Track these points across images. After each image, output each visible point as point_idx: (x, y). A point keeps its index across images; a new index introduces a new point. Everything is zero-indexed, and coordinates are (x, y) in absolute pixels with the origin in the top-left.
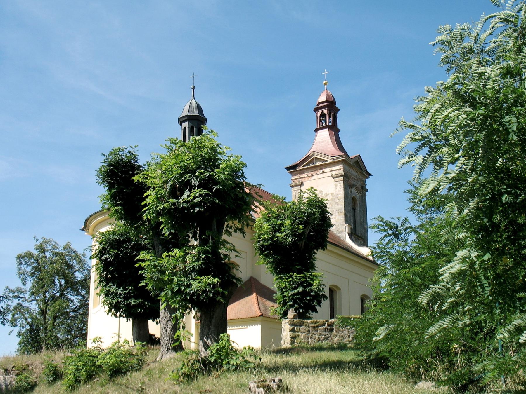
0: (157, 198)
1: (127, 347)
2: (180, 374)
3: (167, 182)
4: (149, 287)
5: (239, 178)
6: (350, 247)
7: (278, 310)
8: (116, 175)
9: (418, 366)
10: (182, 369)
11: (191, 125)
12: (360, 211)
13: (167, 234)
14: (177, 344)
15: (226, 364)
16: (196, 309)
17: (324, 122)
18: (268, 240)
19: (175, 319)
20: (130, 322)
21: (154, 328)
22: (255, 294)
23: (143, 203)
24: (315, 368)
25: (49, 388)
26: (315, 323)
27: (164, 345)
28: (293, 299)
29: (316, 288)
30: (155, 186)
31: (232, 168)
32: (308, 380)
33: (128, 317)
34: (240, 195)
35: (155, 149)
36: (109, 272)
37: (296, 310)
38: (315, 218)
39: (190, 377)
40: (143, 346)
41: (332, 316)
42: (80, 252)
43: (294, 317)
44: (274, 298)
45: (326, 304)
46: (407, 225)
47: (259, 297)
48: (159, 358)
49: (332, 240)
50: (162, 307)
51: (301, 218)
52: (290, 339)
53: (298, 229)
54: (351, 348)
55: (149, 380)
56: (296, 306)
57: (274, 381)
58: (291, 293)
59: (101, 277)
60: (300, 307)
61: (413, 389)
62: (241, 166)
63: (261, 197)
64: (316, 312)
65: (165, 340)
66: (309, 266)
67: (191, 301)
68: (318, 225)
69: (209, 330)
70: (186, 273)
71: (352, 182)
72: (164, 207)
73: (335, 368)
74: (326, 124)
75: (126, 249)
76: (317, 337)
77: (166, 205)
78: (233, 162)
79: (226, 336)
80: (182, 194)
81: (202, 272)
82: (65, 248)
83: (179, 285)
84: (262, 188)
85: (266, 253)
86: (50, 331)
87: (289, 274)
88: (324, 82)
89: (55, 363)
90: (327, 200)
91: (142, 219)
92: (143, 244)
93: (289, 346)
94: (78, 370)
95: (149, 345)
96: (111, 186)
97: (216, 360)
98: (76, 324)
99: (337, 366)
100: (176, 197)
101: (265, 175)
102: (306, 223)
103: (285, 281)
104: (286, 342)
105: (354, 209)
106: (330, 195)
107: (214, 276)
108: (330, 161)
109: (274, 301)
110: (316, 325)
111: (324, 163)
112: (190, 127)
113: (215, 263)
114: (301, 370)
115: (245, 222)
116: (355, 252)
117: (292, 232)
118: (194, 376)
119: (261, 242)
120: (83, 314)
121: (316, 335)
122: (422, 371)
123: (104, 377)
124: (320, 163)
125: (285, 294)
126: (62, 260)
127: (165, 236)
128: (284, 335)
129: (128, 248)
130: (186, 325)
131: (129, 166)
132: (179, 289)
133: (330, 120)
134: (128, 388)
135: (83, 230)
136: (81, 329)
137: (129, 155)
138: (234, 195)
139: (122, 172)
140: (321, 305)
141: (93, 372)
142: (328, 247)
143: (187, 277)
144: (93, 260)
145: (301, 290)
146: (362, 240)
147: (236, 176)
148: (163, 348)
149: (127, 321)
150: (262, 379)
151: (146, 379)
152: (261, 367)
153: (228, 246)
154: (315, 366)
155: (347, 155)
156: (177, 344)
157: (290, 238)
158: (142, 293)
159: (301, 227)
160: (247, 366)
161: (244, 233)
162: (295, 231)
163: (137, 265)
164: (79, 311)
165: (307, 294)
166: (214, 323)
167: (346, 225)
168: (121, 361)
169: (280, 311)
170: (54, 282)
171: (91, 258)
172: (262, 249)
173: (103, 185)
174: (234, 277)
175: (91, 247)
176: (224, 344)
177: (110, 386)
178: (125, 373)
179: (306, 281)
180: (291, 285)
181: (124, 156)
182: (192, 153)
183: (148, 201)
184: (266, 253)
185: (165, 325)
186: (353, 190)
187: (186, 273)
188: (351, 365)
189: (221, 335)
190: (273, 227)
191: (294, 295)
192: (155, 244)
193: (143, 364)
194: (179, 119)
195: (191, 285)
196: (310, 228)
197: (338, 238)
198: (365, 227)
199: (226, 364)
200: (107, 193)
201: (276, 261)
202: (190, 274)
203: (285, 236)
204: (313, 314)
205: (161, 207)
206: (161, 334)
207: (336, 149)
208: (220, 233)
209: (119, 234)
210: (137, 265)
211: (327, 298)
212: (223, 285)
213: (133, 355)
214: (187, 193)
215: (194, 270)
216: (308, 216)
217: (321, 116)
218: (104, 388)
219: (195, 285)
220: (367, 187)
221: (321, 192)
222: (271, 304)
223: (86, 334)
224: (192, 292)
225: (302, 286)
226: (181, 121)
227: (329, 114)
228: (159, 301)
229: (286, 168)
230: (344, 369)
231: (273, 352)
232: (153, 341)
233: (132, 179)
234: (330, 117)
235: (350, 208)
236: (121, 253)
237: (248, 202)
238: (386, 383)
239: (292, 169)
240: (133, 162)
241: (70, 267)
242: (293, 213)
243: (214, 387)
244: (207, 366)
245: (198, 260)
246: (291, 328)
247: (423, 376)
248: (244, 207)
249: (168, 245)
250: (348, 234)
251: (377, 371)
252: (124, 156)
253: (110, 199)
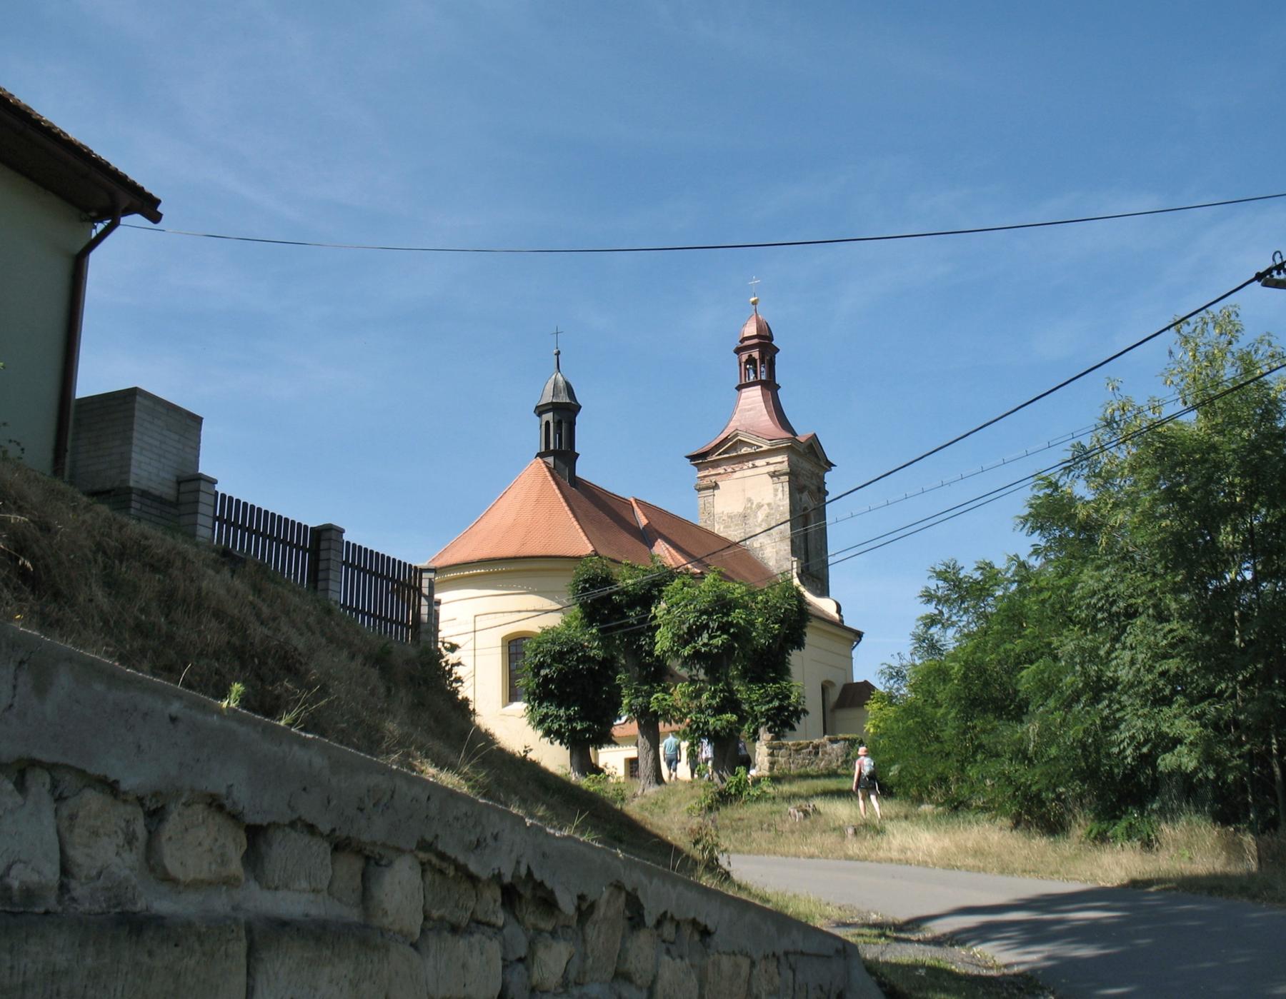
11: (557, 418)
60: (776, 725)
71: (803, 481)
96: (1119, 886)
108: (765, 448)
121: (799, 759)
124: (749, 450)
165: (786, 709)
179: (782, 693)
186: (805, 496)
191: (768, 710)
207: (771, 417)
217: (747, 362)
226: (540, 411)
234: (762, 362)
239: (699, 459)
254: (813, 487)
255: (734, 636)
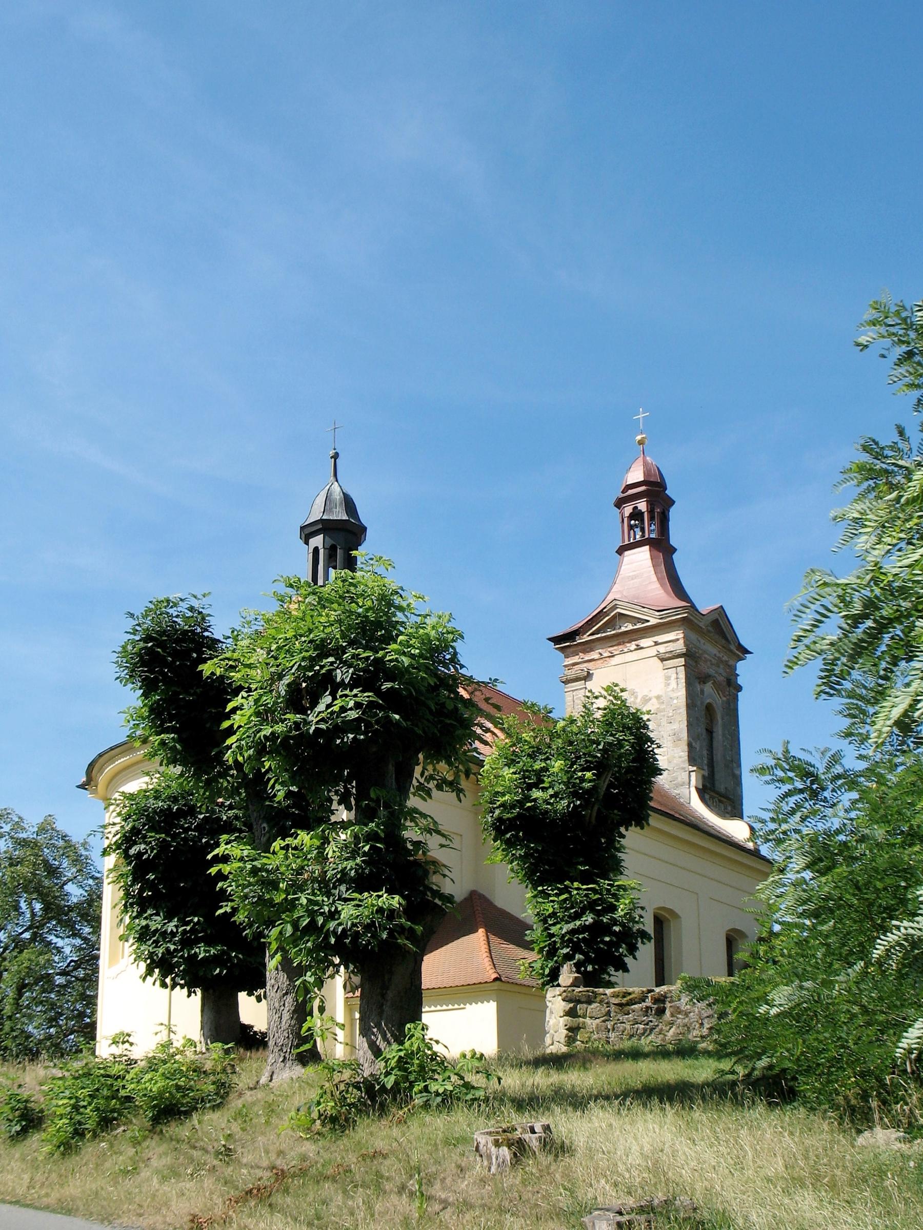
0: (257, 714)
1: (190, 1054)
2: (315, 1115)
3: (281, 677)
4: (241, 917)
5: (446, 666)
6: (701, 819)
7: (537, 965)
8: (163, 663)
9: (865, 1091)
10: (319, 1103)
11: (330, 542)
12: (724, 735)
13: (281, 795)
14: (307, 1047)
15: (421, 1092)
16: (351, 967)
17: (638, 530)
18: (513, 807)
19: (302, 992)
20: (197, 998)
21: (252, 1011)
22: (481, 931)
23: (226, 724)
24: (624, 1100)
25: (13, 1151)
26: (624, 997)
27: (276, 1050)
28: (570, 940)
29: (626, 914)
30: (253, 686)
31: (430, 641)
32: (611, 1125)
33: (191, 986)
34: (450, 706)
35: (252, 600)
36: (147, 885)
37: (578, 965)
38: (621, 756)
39: (337, 1123)
40: (227, 1052)
41: (661, 980)
42: (77, 837)
43: (575, 984)
44: (528, 938)
45: (646, 950)
46: (838, 770)
47: (491, 937)
48: (264, 1080)
49: (659, 802)
50: (272, 963)
51: (589, 754)
52: (566, 1032)
53: (582, 780)
54: (708, 1054)
55: (243, 1130)
56: (578, 956)
57: (533, 1131)
58: (566, 928)
59: (127, 894)
60: (588, 960)
61: (853, 1147)
62: (450, 636)
63: (498, 708)
64: (626, 970)
65: (279, 1037)
66: (607, 864)
67: (339, 949)
68: (629, 770)
69: (380, 1014)
70: (327, 886)
71: (705, 668)
72: (273, 733)
73: (671, 1100)
74: (643, 536)
75: (186, 830)
76: (628, 1027)
77: (279, 728)
78: (433, 628)
79: (420, 1027)
80: (314, 703)
81: (363, 883)
82: (42, 829)
83: (312, 914)
84: (500, 687)
85: (508, 836)
86: (10, 1018)
87: (561, 883)
88: (639, 438)
89: (25, 1094)
90: (649, 712)
91: (222, 763)
92: (225, 818)
93: (564, 1049)
94: (76, 1108)
95: (242, 1050)
96: (149, 688)
97: (396, 1083)
98: (70, 1003)
99: (675, 1094)
100: (303, 711)
101: (503, 657)
102: (600, 767)
103: (553, 901)
104: (555, 1039)
105: (710, 732)
106: (654, 700)
107: (390, 892)
108: (653, 621)
109: (527, 946)
110: (624, 1000)
111: (639, 626)
112: (327, 546)
113: (394, 865)
114: (592, 1104)
115: (461, 767)
116: (713, 832)
117: (568, 788)
118: (347, 1120)
119: (497, 812)
120: (83, 980)
122: (874, 1104)
123: (139, 1122)
124: (629, 627)
125: (553, 930)
126: (36, 855)
127: (277, 799)
128: (551, 1023)
129: (189, 829)
130: (326, 1005)
131: (193, 641)
132: (313, 922)
133: (653, 527)
134: (195, 1147)
135: (82, 786)
136: (82, 1015)
137: (190, 614)
138: (436, 704)
139: (176, 654)
140: (637, 954)
141: (113, 1111)
142: (651, 821)
143: (328, 894)
144: (106, 858)
145: (591, 920)
146: (730, 805)
147: (440, 662)
148: (272, 1056)
149: (189, 996)
150: (504, 1126)
151: (235, 1127)
152: (501, 1098)
153: (423, 822)
154: (625, 1095)
155: (693, 606)
156: (307, 1047)
157: (565, 802)
158: (224, 931)
159: (588, 775)
160: (469, 1097)
161: (459, 791)
162: (574, 785)
163: (213, 871)
164: (75, 973)
165: (605, 929)
166: (393, 999)
167: (691, 768)
168: (178, 1088)
169: (542, 968)
170: (17, 908)
171: (105, 853)
172: (500, 828)
173: (130, 686)
174: (437, 894)
175: (104, 827)
176: (416, 1046)
177: (153, 1143)
178: (188, 1114)
179: (601, 900)
180: (567, 909)
181: (177, 616)
182: (335, 611)
183: (237, 719)
184: (508, 836)
185: (277, 1005)
186: (708, 688)
187: (325, 885)
188: (707, 1090)
189: (408, 1025)
190: (524, 777)
191: (573, 932)
192: (253, 819)
193: (227, 1093)
194: (302, 528)
195: (337, 912)
196: (609, 778)
197: (673, 800)
198: (737, 772)
199: (421, 1092)
200: (139, 703)
201: (532, 855)
202: (335, 888)
203: (551, 796)
204: (616, 976)
205: (267, 731)
206: (269, 1024)
207: (662, 585)
208: (403, 789)
209: (169, 798)
210: (213, 871)
211: (649, 939)
212: (414, 910)
213: (205, 1072)
214: (327, 699)
215: (344, 877)
216: (604, 751)
217: (631, 517)
218: (139, 1149)
219: (347, 912)
220: (740, 681)
221: (633, 693)
222: (520, 952)
223: (93, 1026)
224: (340, 929)
225: (593, 911)
226: (307, 533)
227: (651, 512)
228: (263, 948)
229: (550, 639)
230: (691, 1099)
231: (528, 1063)
232: (250, 1040)
233: (200, 668)
234: (652, 518)
235: (701, 730)
236: (173, 839)
237: (466, 719)
238: (791, 1133)
239: (565, 641)
240: (199, 630)
241: (53, 872)
242: (571, 743)
243: (395, 1144)
244: (375, 1098)
245: (354, 854)
246: (567, 1008)
247: (876, 1116)
248: (459, 732)
249: (283, 822)
250: (697, 788)
251: (769, 1104)
252: (177, 616)
253: (148, 717)
254: (720, 679)
255: (392, 700)
